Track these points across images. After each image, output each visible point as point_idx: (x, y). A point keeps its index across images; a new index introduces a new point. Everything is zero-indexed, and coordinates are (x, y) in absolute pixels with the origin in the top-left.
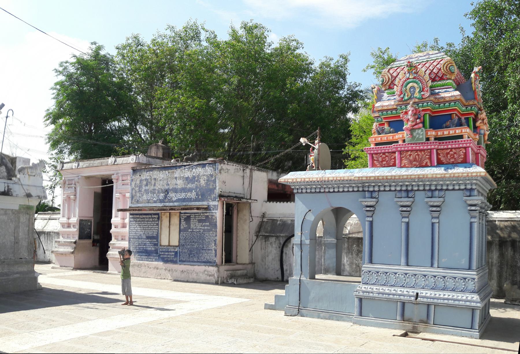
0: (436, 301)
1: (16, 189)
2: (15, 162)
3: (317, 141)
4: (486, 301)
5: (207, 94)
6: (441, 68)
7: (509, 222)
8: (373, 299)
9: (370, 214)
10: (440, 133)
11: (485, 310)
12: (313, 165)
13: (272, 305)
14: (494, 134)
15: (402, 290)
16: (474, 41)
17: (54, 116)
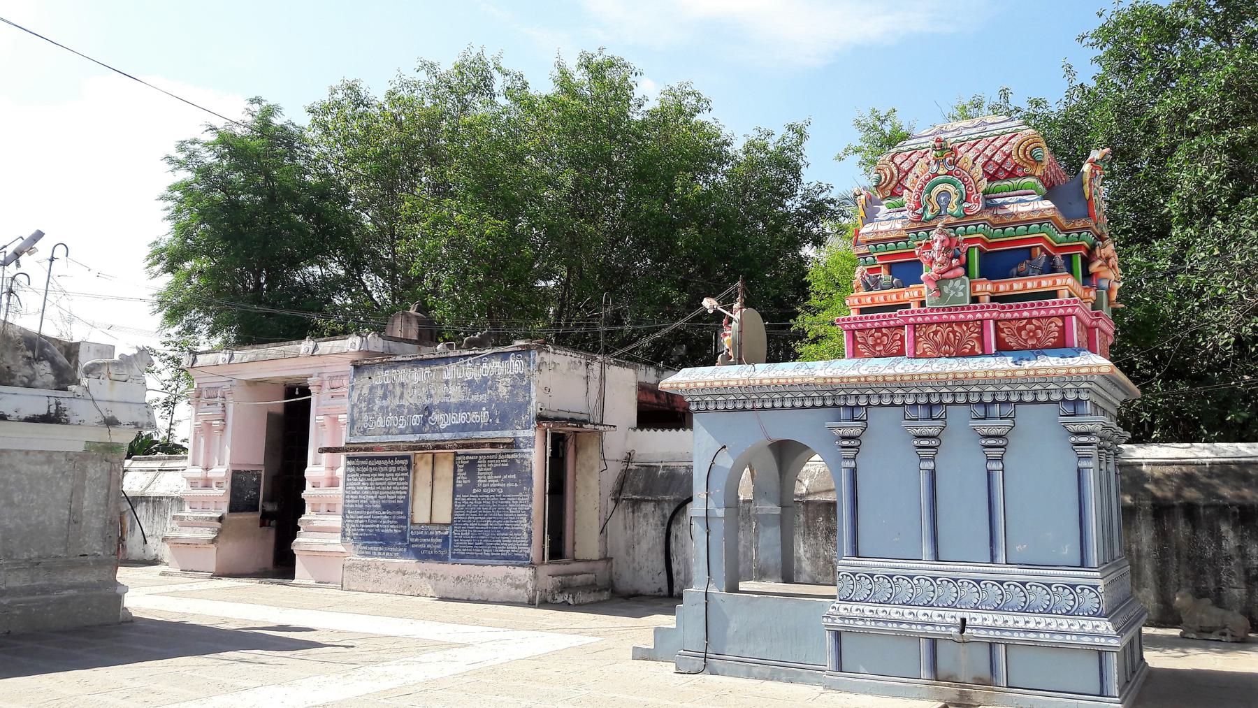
0: (1007, 635)
1: (77, 409)
2: (76, 353)
3: (738, 303)
4: (1132, 632)
5: (509, 208)
6: (1011, 152)
7: (1174, 467)
8: (864, 633)
9: (851, 453)
10: (1003, 287)
11: (1132, 653)
12: (731, 353)
13: (648, 649)
14: (1134, 288)
15: (929, 612)
16: (1095, 95)
17: (170, 255)
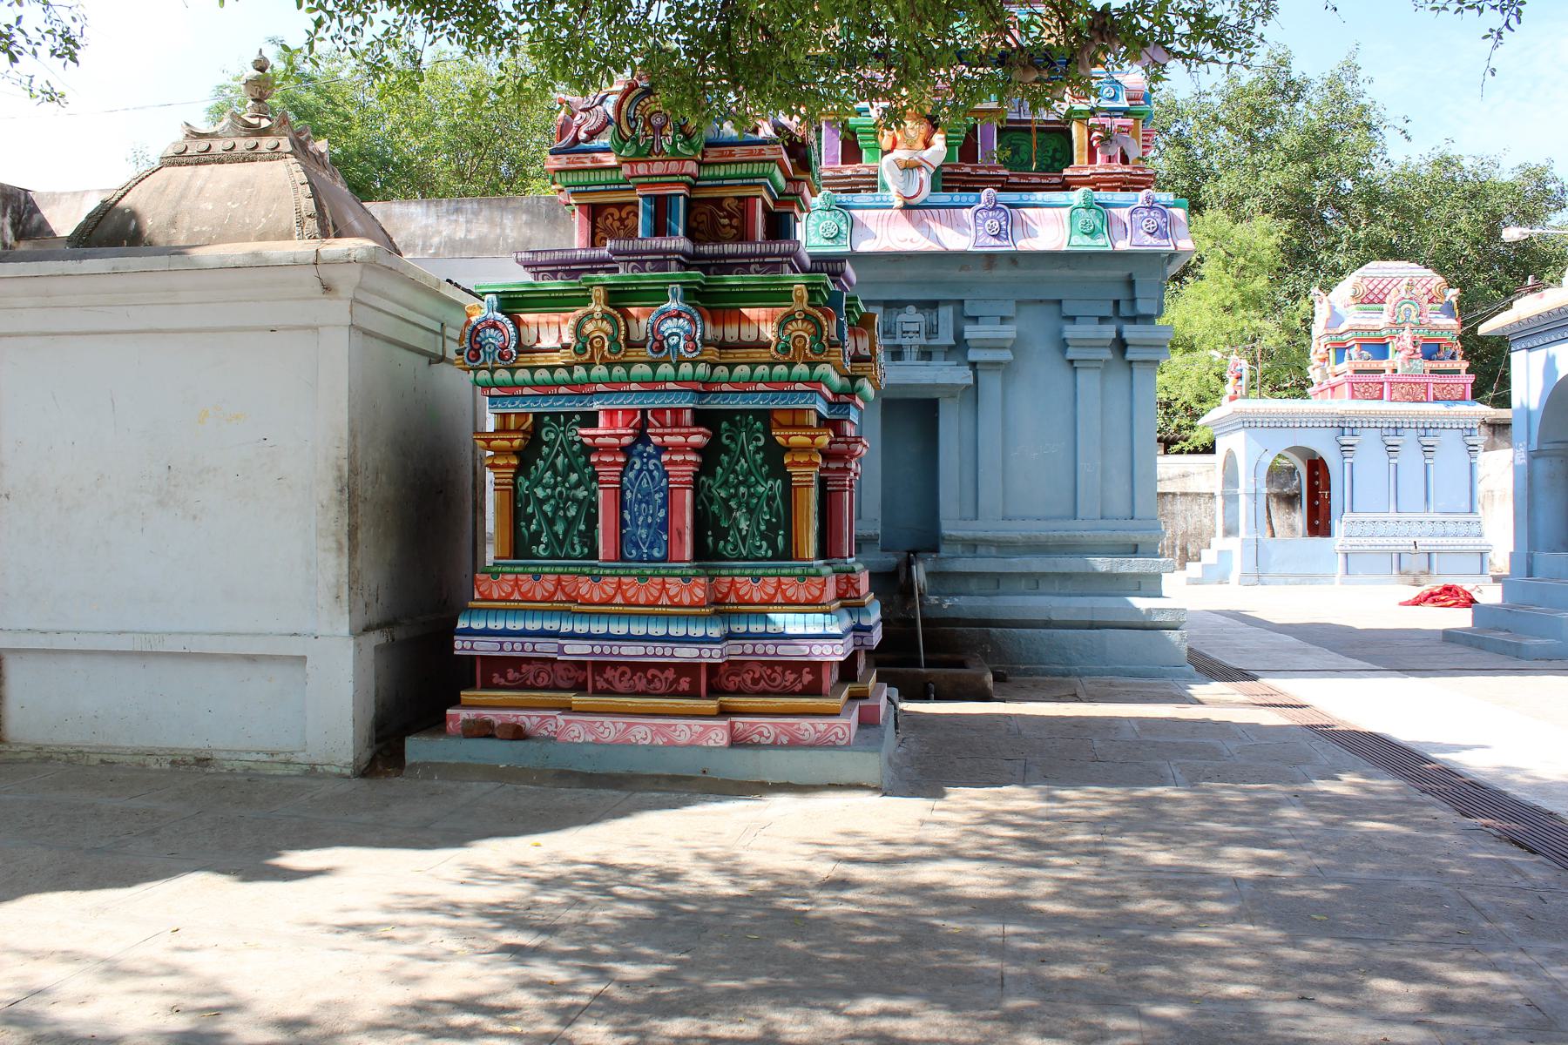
0: (1440, 548)
